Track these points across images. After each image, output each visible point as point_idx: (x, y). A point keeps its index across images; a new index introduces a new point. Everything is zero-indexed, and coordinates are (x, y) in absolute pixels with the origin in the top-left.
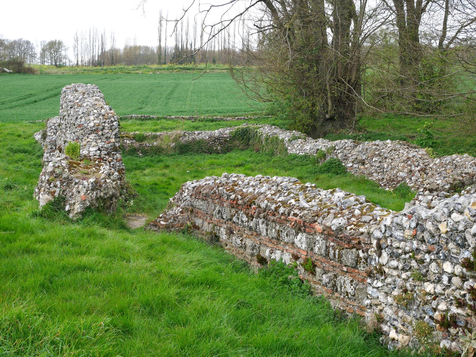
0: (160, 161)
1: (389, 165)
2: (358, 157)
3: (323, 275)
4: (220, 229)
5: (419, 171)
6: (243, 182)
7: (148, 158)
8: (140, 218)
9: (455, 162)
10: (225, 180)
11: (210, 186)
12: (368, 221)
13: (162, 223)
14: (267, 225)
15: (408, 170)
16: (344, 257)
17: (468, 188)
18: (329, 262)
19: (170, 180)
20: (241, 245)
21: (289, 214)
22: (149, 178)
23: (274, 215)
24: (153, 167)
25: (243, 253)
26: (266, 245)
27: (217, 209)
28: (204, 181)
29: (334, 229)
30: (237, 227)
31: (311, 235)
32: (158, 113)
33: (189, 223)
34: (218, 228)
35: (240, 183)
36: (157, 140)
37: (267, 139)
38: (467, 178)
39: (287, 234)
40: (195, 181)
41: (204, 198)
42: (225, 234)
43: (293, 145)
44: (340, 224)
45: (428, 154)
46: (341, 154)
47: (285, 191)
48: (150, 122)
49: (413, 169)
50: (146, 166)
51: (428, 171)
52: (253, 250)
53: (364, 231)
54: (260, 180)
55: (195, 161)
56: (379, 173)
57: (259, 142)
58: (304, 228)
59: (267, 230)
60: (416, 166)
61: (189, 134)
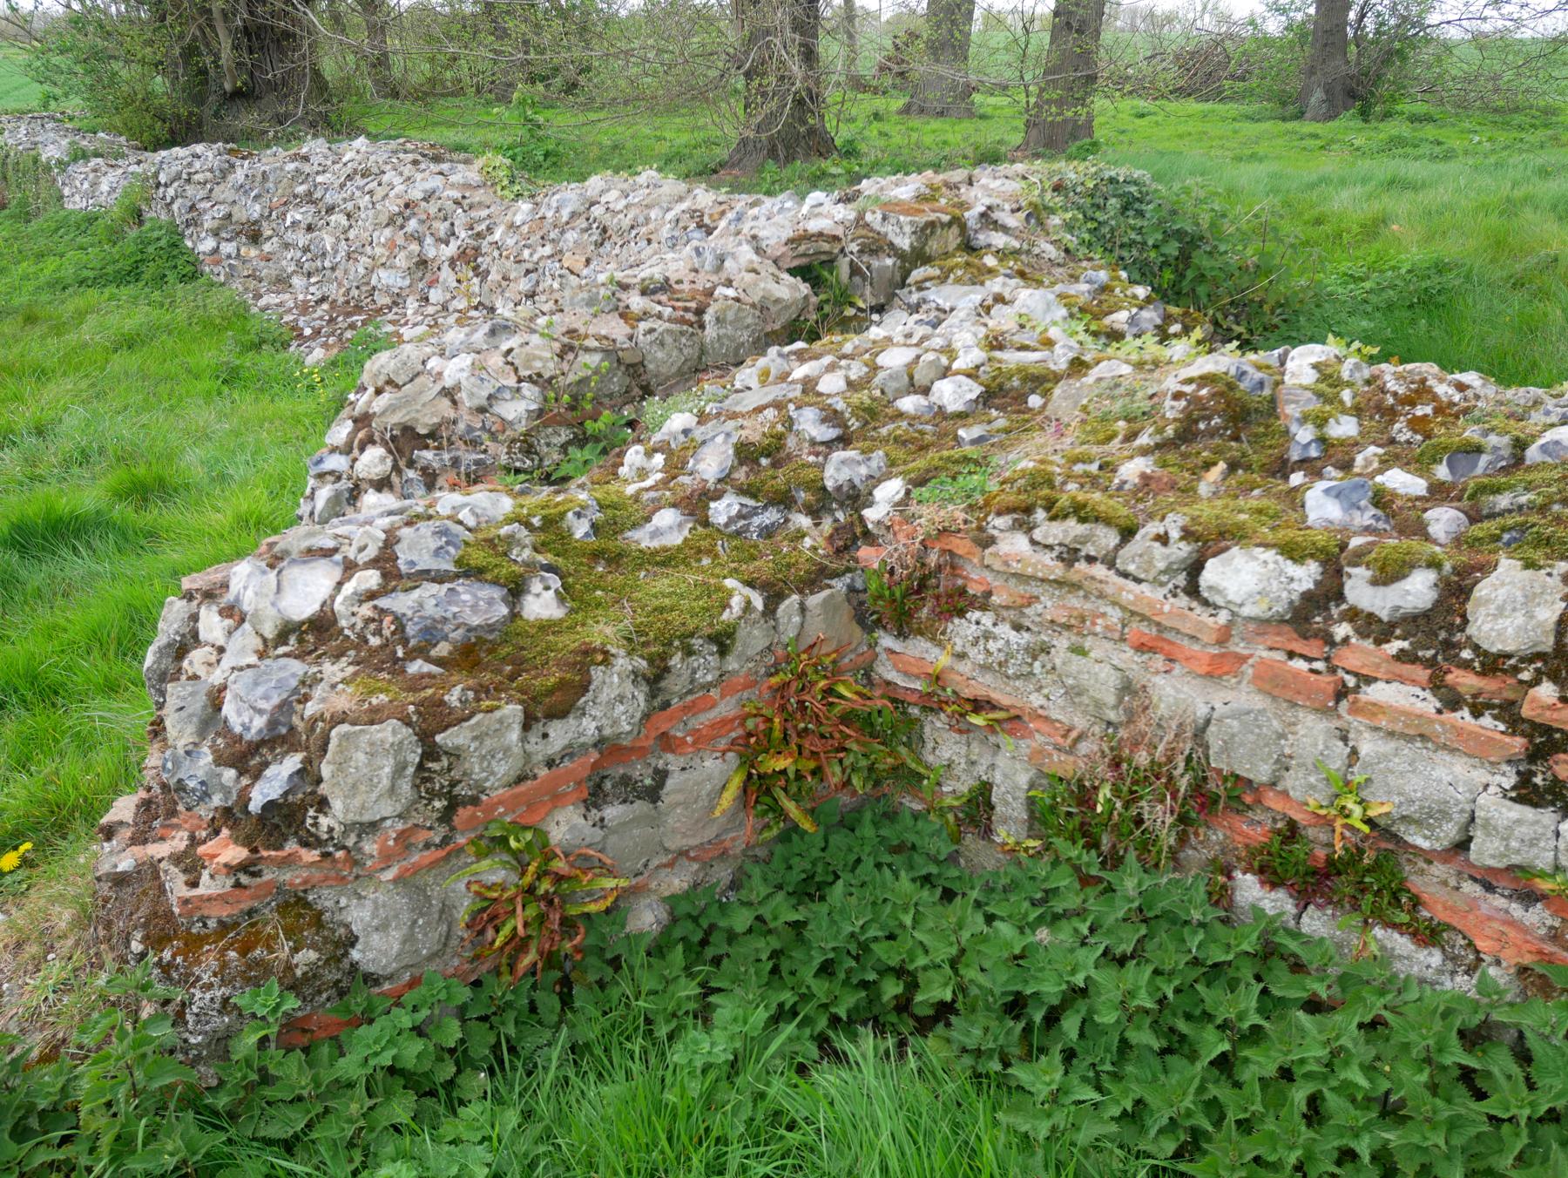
2: (235, 210)
5: (452, 262)
9: (597, 211)
17: (678, 421)
38: (661, 326)
49: (431, 253)
51: (488, 259)
56: (309, 275)
60: (439, 240)
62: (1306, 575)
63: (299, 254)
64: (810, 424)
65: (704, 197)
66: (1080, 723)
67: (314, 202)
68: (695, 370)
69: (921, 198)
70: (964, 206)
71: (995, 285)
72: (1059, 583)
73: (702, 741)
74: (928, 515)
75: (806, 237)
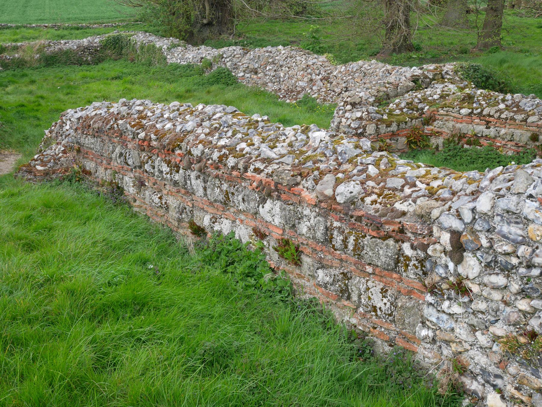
0: (24, 75)
1: (285, 74)
2: (250, 65)
3: (317, 269)
4: (123, 178)
5: (321, 80)
6: (153, 112)
7: (10, 72)
8: (6, 156)
9: (363, 69)
10: (125, 110)
11: (103, 116)
12: (400, 188)
13: (39, 168)
14: (205, 182)
15: (308, 78)
16: (368, 250)
18: (333, 252)
19: (40, 99)
20: (159, 204)
21: (246, 169)
22: (13, 97)
23: (217, 168)
24: (17, 83)
25: (164, 215)
26: (203, 209)
27: (118, 150)
28: (93, 110)
29: (342, 202)
30: (151, 178)
31: (292, 204)
32: (17, 21)
33: (76, 168)
34: (121, 176)
35: (149, 114)
36: (18, 52)
37: (142, 48)
39: (243, 199)
40: (80, 108)
41: (96, 134)
42: (133, 186)
43: (173, 54)
44: (351, 192)
45: (329, 60)
46: (230, 62)
47: (225, 129)
48: (8, 31)
49: (314, 77)
50: (8, 82)
51: (333, 79)
52: (181, 214)
53: (406, 210)
54: (178, 110)
55: (65, 75)
56: (274, 83)
57: (133, 51)
58: (277, 193)
59: (205, 189)
60: (316, 75)
61: (54, 44)
62: (470, 111)
63: (271, 77)
64: (416, 100)
65: (389, 67)
66: (449, 132)
67: (275, 64)
68: (396, 96)
69: (435, 69)
70: (443, 70)
71: (446, 84)
72: (446, 115)
73: (403, 136)
74: (432, 109)
75: (414, 76)
